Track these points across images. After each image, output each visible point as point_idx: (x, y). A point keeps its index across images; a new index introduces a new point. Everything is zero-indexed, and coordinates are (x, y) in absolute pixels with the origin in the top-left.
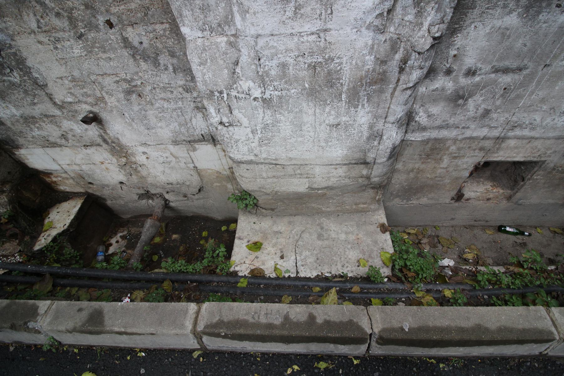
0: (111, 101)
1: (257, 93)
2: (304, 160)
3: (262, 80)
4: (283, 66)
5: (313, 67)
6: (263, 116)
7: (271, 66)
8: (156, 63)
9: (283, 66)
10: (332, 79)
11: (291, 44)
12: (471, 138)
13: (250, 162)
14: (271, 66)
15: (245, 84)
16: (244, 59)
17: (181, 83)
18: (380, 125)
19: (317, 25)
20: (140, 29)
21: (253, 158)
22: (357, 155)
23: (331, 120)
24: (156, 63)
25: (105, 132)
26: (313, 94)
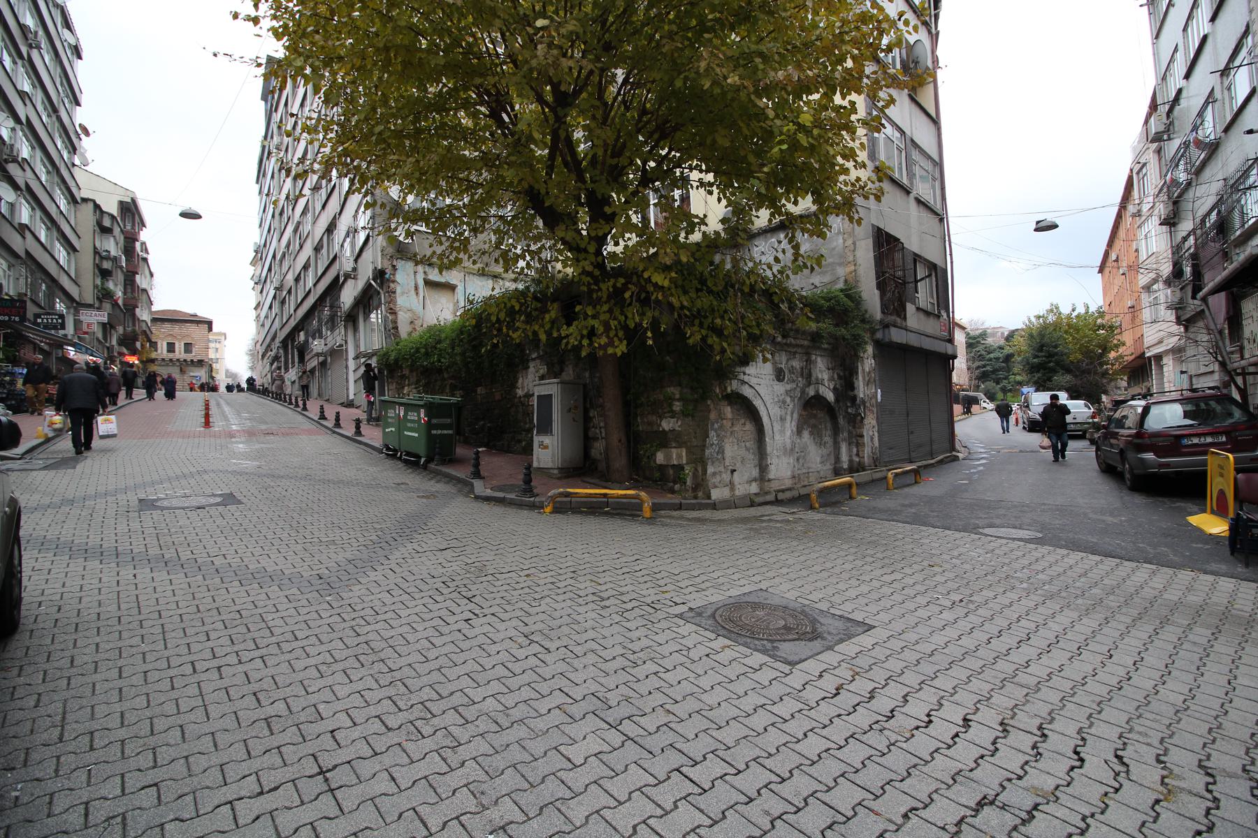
26: (784, 454)
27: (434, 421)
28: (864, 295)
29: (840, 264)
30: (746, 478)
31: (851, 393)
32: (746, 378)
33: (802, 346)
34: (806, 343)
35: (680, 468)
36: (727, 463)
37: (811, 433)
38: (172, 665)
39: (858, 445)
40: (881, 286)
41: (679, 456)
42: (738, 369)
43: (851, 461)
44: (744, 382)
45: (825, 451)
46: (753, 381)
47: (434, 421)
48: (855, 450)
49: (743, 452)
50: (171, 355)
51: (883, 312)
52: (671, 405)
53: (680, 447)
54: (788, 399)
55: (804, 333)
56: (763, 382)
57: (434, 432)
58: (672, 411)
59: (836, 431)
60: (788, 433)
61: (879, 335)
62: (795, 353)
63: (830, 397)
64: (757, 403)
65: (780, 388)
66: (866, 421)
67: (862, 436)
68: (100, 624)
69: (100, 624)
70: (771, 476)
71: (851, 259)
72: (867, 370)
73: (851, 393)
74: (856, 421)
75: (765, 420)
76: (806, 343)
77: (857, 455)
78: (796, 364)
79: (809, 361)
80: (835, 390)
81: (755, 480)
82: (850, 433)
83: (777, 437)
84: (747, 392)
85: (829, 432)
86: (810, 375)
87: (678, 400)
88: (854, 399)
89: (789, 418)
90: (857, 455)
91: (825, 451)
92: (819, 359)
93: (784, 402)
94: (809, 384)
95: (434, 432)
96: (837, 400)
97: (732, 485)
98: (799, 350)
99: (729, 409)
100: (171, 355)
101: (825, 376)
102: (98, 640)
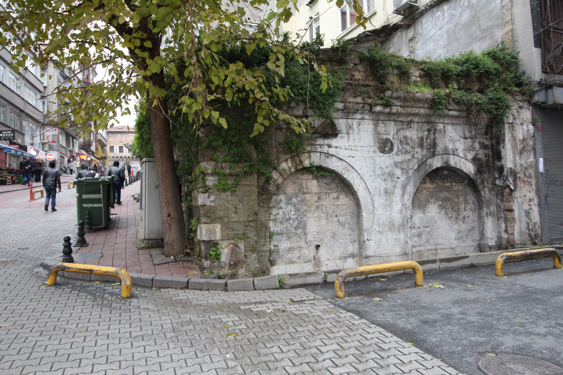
0: (326, 240)
1: (377, 229)
2: (360, 293)
3: (379, 225)
4: (384, 222)
5: (389, 222)
6: (379, 236)
7: (381, 222)
8: (344, 227)
9: (384, 222)
10: (394, 225)
11: (385, 217)
12: (428, 250)
13: (374, 256)
14: (381, 222)
15: (375, 227)
16: (376, 220)
17: (349, 233)
18: (406, 239)
19: (389, 213)
20: (343, 217)
21: (374, 254)
22: (404, 251)
23: (395, 238)
24: (344, 227)
25: (317, 253)
26: (390, 229)
27: (84, 196)
28: (522, 56)
29: (498, 26)
30: (338, 254)
31: (498, 164)
32: (332, 151)
33: (417, 115)
34: (422, 111)
35: (212, 244)
36: (310, 237)
37: (442, 207)
38: (142, 348)
39: (506, 220)
40: (539, 42)
41: (213, 232)
42: (320, 141)
43: (499, 238)
44: (328, 155)
45: (464, 227)
46: (342, 154)
47: (84, 196)
48: (503, 226)
49: (334, 227)
50: (121, 154)
51: (544, 71)
52: (204, 181)
53: (213, 221)
54: (398, 172)
55: (419, 100)
56: (357, 154)
57: (85, 205)
58: (205, 186)
59: (480, 204)
60: (397, 207)
61: (539, 98)
62: (410, 122)
63: (469, 168)
64: (349, 176)
65: (386, 160)
66: (517, 194)
67: (511, 211)
68: (99, 320)
69: (99, 320)
70: (369, 252)
71: (508, 18)
72: (520, 136)
73: (498, 164)
74: (504, 193)
75: (362, 193)
76: (422, 111)
77: (506, 231)
78: (413, 134)
79: (432, 130)
80: (475, 160)
81: (353, 256)
82: (498, 206)
83: (380, 212)
84: (333, 164)
85: (471, 206)
86: (434, 145)
87: (212, 174)
88: (501, 169)
89: (398, 191)
90: (506, 231)
91: (464, 227)
92: (449, 128)
93: (391, 175)
94: (433, 155)
95: (85, 205)
96: (479, 171)
97: (317, 261)
98: (416, 119)
99: (315, 182)
100: (121, 154)
101: (460, 146)
102: (98, 328)
